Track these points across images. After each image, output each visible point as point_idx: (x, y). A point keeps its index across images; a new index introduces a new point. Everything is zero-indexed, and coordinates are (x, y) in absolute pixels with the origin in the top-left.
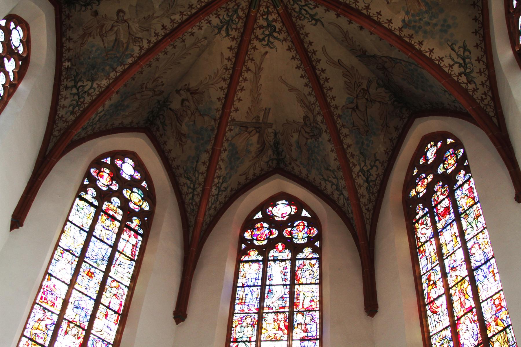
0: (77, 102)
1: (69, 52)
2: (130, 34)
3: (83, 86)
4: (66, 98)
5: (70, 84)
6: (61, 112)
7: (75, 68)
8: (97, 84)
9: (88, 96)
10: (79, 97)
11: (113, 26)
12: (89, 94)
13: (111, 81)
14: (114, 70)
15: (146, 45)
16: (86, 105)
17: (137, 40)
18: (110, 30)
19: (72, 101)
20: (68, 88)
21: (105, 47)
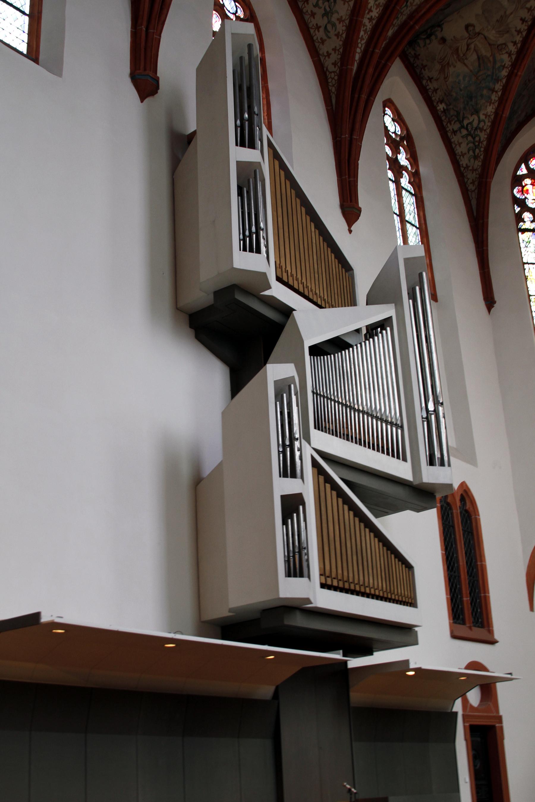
0: (474, 143)
1: (436, 93)
2: (490, 44)
3: (471, 123)
4: (460, 144)
5: (456, 126)
6: (464, 162)
7: (451, 107)
8: (483, 114)
9: (481, 131)
10: (472, 137)
11: (468, 45)
12: (481, 130)
13: (496, 104)
14: (493, 90)
15: (513, 49)
16: (485, 143)
17: (501, 47)
18: (467, 49)
19: (467, 144)
20: (456, 131)
21: (471, 71)
